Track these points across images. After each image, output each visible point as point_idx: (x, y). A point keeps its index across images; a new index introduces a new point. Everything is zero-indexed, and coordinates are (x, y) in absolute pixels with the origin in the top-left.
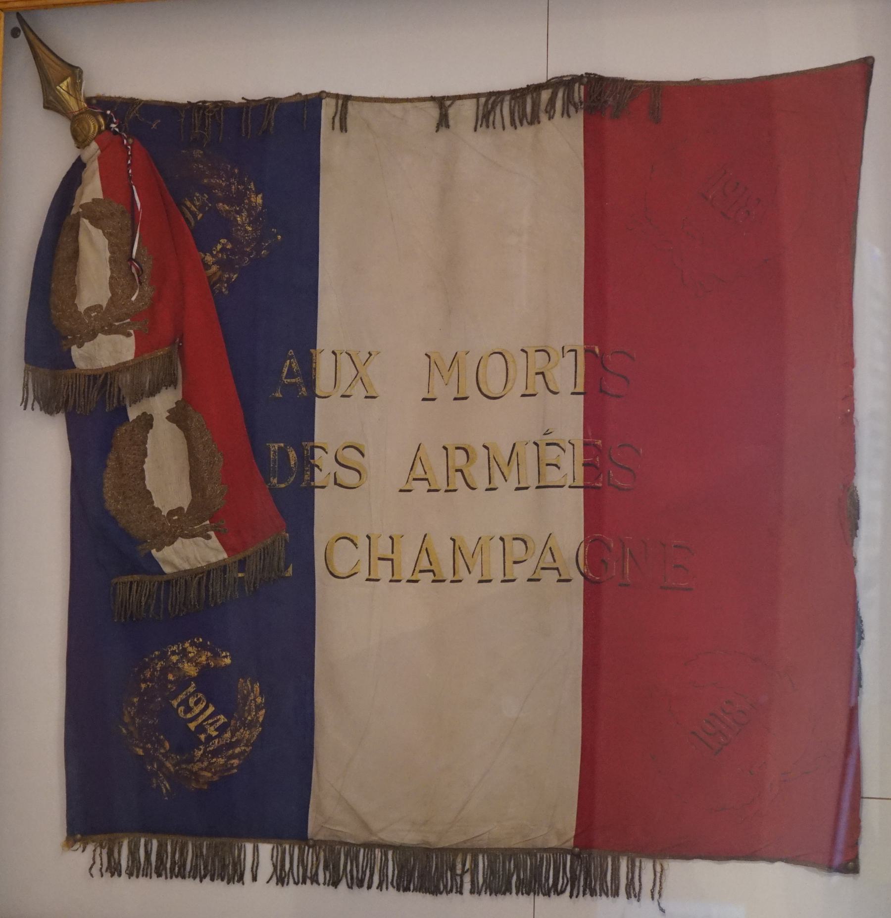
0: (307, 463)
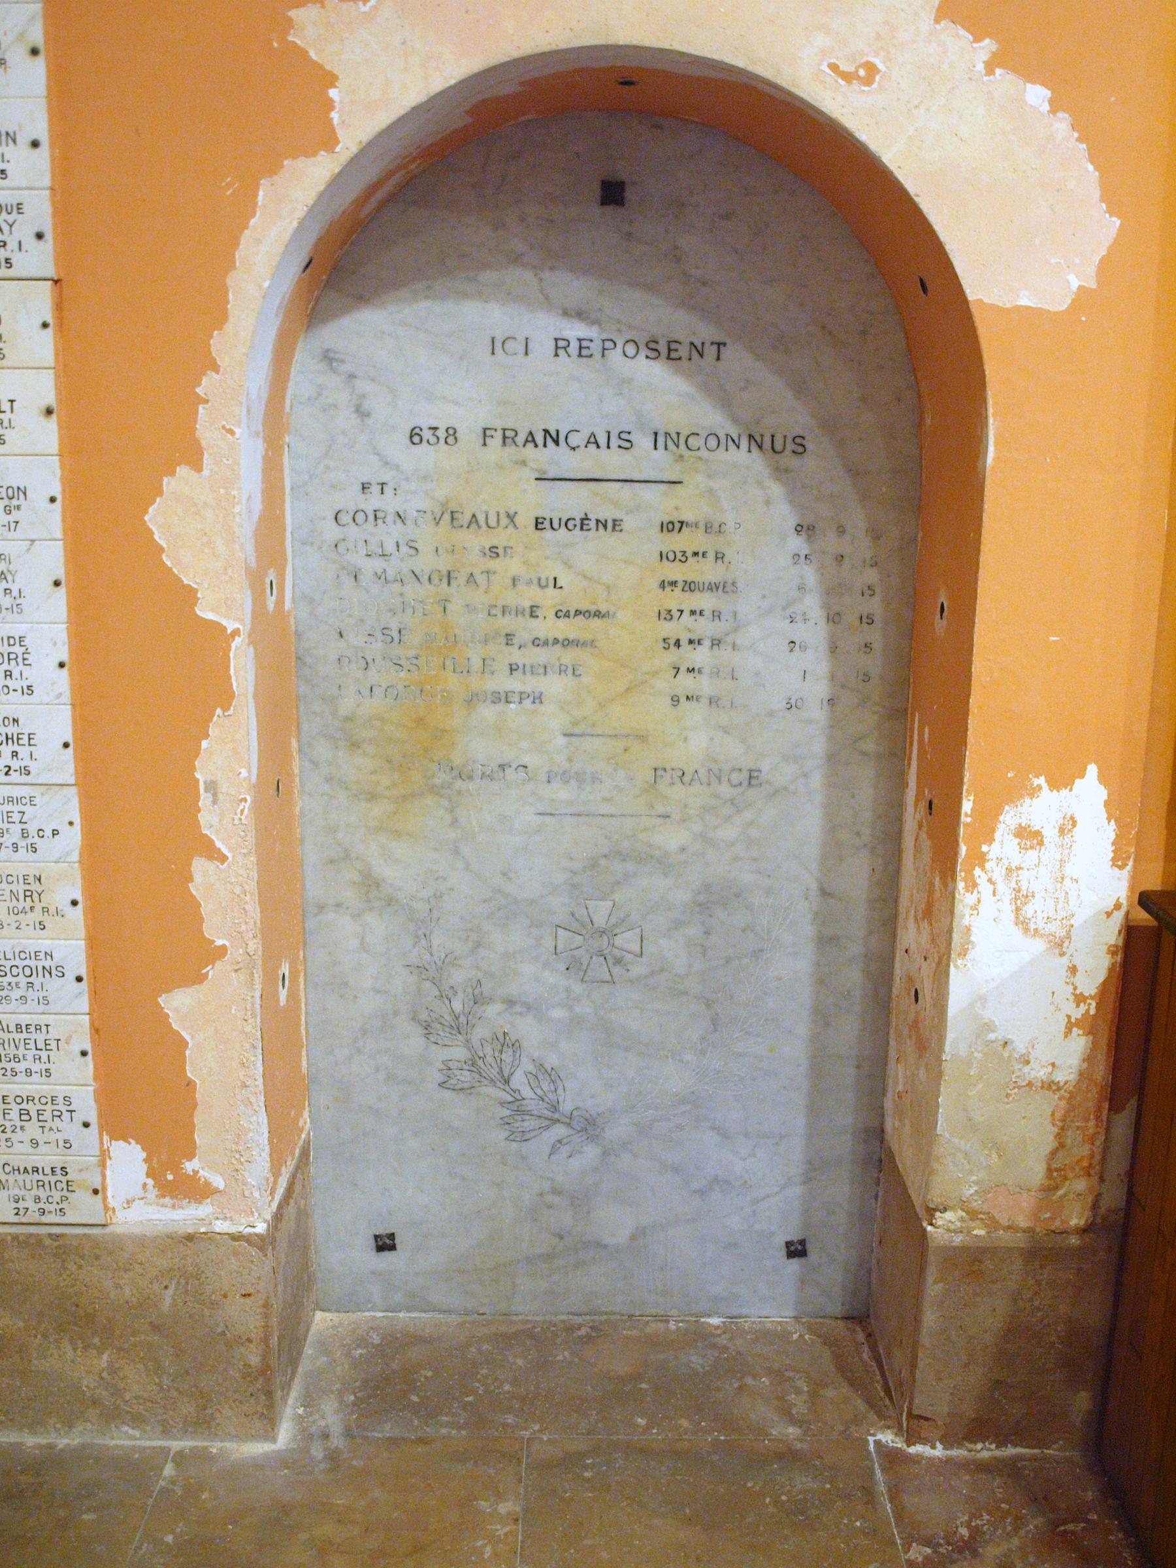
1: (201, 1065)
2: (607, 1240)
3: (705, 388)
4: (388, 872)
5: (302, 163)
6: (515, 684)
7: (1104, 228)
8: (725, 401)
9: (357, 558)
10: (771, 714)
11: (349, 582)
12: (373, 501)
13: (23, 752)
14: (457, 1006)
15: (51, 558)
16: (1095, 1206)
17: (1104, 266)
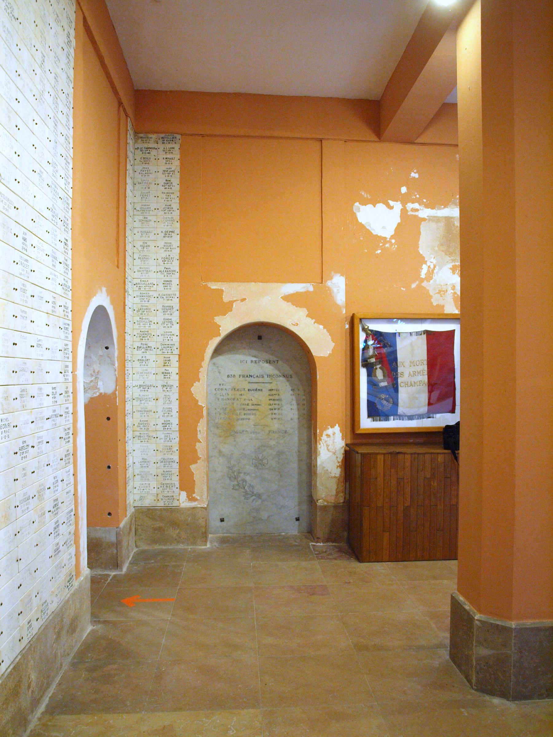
0: (397, 374)
1: (196, 478)
2: (263, 518)
3: (276, 368)
4: (223, 450)
5: (216, 338)
6: (245, 417)
7: (333, 345)
8: (279, 370)
9: (218, 396)
10: (288, 421)
11: (217, 400)
12: (222, 387)
13: (170, 426)
14: (235, 474)
15: (177, 396)
16: (345, 498)
17: (333, 350)
